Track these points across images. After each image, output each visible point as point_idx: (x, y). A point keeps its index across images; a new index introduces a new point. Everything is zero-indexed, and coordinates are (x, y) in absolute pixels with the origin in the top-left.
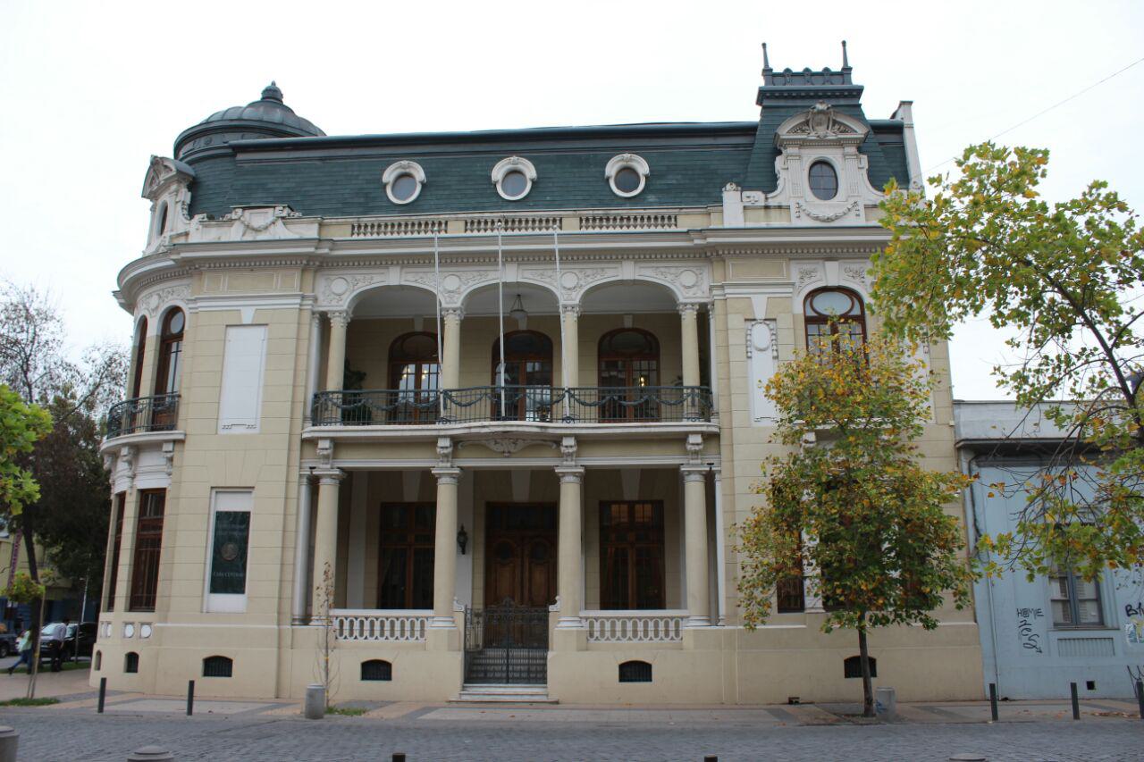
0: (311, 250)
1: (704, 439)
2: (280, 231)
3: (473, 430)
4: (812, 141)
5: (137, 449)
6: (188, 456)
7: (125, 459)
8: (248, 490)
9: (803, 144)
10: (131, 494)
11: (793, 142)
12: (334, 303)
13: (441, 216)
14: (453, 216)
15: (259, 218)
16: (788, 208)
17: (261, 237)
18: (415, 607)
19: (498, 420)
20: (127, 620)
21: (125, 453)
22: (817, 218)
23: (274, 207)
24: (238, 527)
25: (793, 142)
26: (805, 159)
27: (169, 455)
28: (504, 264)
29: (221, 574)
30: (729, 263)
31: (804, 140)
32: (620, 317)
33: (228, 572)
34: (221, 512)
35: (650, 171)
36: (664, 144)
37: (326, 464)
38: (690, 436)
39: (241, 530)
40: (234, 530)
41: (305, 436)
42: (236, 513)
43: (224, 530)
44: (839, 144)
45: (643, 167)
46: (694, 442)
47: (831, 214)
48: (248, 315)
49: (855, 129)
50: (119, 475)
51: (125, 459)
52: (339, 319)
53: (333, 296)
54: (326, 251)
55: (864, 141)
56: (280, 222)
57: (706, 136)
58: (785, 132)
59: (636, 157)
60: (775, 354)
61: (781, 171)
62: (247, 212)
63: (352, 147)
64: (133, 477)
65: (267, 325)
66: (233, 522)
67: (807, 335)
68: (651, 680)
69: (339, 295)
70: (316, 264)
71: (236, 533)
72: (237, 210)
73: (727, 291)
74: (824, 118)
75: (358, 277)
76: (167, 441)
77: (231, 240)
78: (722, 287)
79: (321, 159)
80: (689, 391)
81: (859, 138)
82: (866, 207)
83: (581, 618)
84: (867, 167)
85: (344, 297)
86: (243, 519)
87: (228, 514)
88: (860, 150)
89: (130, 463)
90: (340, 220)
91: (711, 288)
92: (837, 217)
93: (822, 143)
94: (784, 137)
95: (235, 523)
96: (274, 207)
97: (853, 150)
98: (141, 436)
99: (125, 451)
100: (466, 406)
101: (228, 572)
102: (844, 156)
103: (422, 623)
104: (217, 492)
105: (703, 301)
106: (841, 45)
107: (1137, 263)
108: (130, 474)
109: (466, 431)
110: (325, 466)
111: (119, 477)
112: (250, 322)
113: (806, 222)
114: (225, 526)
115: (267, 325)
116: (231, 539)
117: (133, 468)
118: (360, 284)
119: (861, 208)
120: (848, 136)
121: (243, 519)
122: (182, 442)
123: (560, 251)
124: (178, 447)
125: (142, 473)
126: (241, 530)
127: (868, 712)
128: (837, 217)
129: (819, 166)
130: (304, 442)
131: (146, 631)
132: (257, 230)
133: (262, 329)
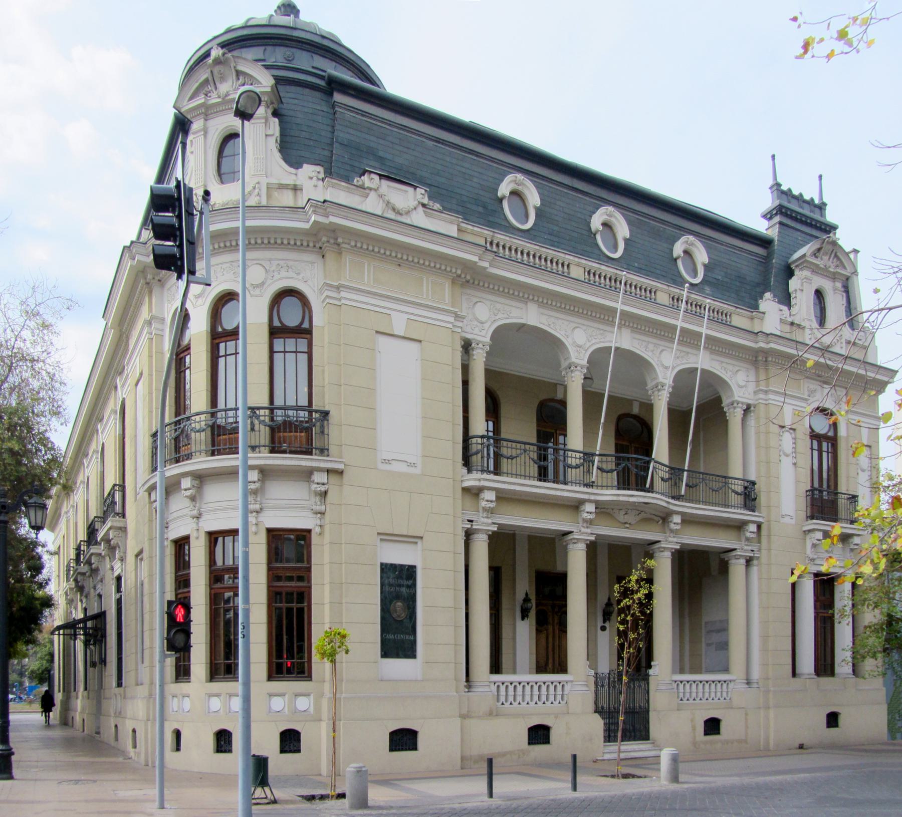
1: (497, 497)
2: (419, 218)
3: (621, 498)
5: (201, 478)
6: (342, 495)
7: (188, 493)
8: (414, 539)
10: (197, 538)
12: (476, 331)
13: (567, 257)
14: (576, 259)
15: (406, 198)
17: (399, 218)
18: (553, 672)
19: (642, 490)
21: (189, 486)
23: (415, 187)
24: (406, 583)
27: (323, 488)
28: (620, 328)
29: (391, 637)
30: (347, 258)
32: (630, 402)
33: (398, 638)
34: (386, 564)
35: (541, 204)
36: (662, 217)
37: (488, 517)
38: (315, 473)
39: (408, 587)
40: (400, 586)
41: (466, 484)
43: (390, 585)
45: (534, 198)
48: (399, 325)
50: (175, 515)
51: (188, 493)
52: (480, 351)
53: (476, 323)
54: (486, 265)
56: (420, 209)
57: (717, 230)
59: (699, 244)
60: (794, 461)
62: (385, 183)
63: (743, 240)
64: (198, 517)
66: (399, 577)
69: (484, 318)
70: (468, 279)
71: (404, 590)
72: (373, 176)
73: (771, 396)
75: (498, 306)
76: (320, 470)
77: (363, 209)
78: (766, 392)
83: (490, 682)
85: (486, 326)
86: (409, 573)
87: (393, 567)
89: (193, 499)
90: (476, 229)
91: (755, 393)
95: (402, 578)
96: (415, 187)
98: (202, 462)
99: (186, 483)
100: (608, 472)
101: (398, 638)
103: (563, 686)
104: (381, 540)
105: (750, 402)
106: (770, 159)
107: (3, 361)
108: (195, 512)
109: (615, 498)
110: (486, 520)
111: (175, 519)
114: (392, 581)
115: (420, 341)
116: (398, 597)
117: (197, 505)
118: (500, 316)
121: (409, 573)
122: (340, 473)
123: (682, 328)
124: (334, 479)
125: (210, 511)
126: (408, 587)
130: (466, 490)
132: (399, 213)
133: (414, 346)
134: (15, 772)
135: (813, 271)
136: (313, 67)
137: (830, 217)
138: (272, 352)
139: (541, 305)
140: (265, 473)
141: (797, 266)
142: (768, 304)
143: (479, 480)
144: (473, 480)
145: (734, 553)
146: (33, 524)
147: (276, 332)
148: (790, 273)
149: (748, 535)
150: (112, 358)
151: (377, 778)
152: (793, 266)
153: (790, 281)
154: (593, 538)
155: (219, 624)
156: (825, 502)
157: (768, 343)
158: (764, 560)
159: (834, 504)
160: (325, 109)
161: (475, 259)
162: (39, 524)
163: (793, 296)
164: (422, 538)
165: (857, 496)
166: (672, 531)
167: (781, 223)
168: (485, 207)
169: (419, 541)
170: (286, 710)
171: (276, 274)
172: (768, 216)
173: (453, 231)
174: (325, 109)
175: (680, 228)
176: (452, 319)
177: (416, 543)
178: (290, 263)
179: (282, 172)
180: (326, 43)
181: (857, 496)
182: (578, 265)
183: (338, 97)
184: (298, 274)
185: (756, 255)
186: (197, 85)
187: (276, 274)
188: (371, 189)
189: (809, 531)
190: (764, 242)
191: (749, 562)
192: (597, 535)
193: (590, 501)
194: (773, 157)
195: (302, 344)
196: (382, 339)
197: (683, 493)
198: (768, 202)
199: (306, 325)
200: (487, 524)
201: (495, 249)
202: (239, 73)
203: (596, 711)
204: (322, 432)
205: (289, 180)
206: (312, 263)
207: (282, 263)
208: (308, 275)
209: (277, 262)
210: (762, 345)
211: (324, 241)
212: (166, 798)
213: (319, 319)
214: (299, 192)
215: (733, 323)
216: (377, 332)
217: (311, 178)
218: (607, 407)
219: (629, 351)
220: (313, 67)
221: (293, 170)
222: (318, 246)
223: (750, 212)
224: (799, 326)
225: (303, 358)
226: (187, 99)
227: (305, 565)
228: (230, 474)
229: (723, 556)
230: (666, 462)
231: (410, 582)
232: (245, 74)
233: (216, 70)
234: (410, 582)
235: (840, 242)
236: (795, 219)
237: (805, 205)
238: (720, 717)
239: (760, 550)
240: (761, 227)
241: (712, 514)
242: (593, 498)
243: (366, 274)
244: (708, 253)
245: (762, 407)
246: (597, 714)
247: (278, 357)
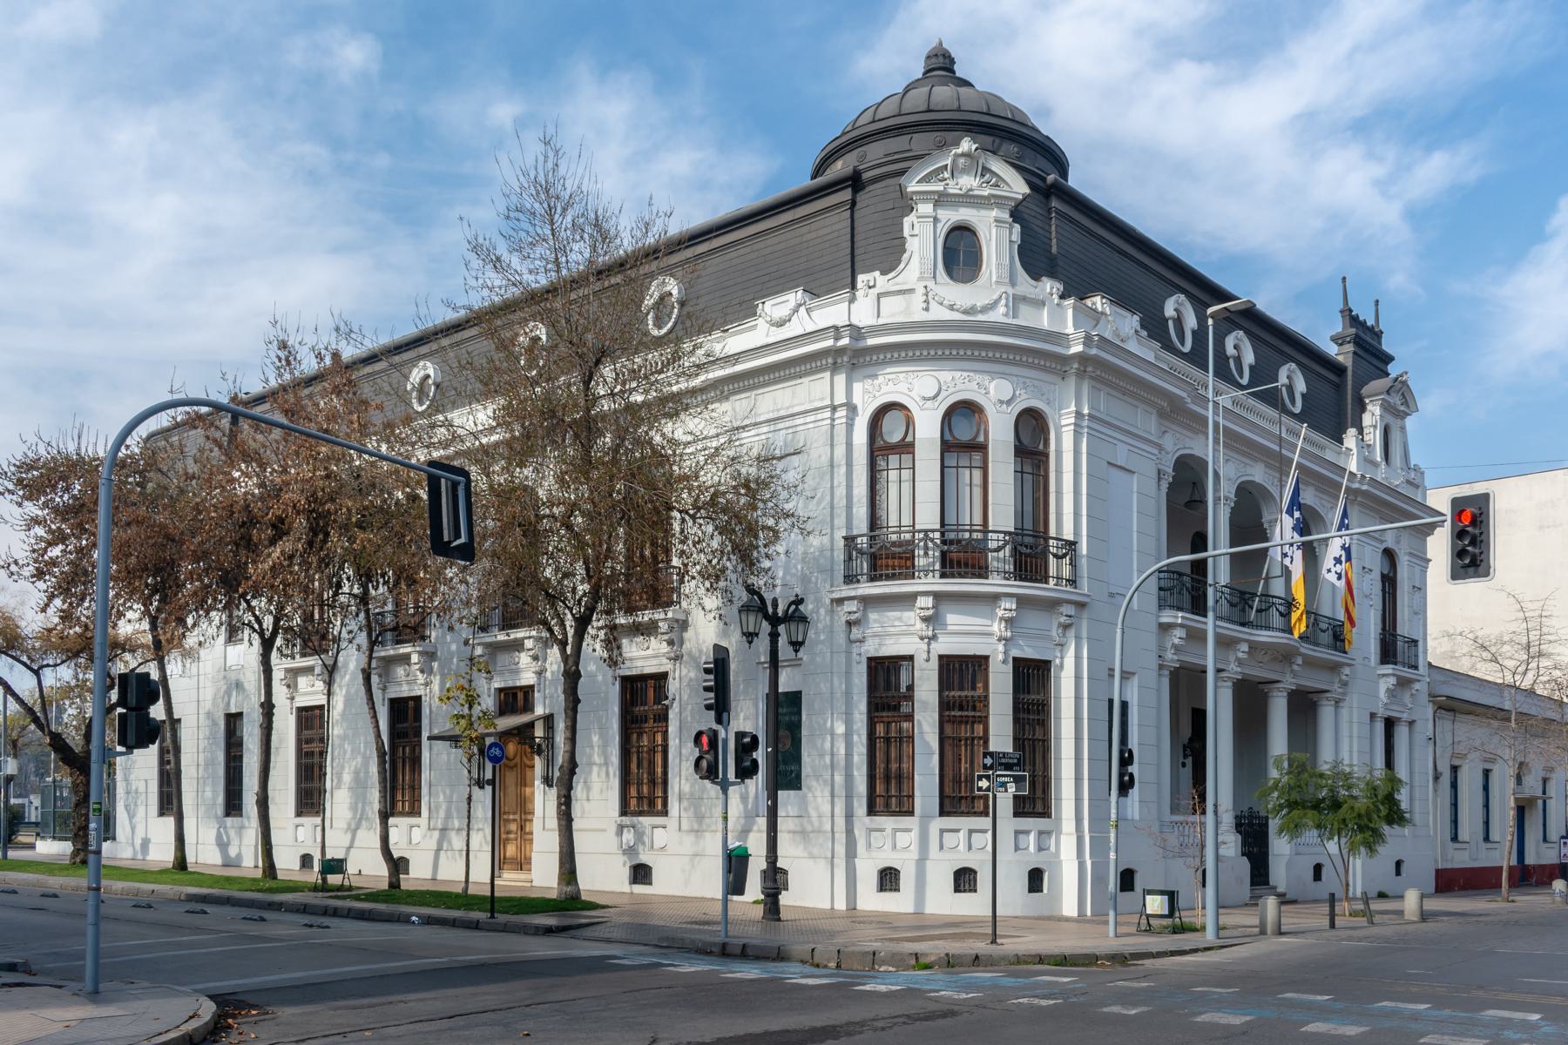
2: (1132, 346)
35: (1052, 275)
138: (943, 467)
140: (938, 597)
147: (947, 447)
150: (407, 344)
161: (1184, 395)
167: (1355, 353)
172: (1338, 340)
173: (1150, 357)
175: (1282, 352)
190: (1339, 370)
195: (977, 457)
199: (981, 439)
202: (986, 170)
218: (1088, 475)
225: (977, 474)
227: (979, 692)
228: (908, 599)
232: (994, 174)
236: (1367, 351)
247: (951, 473)
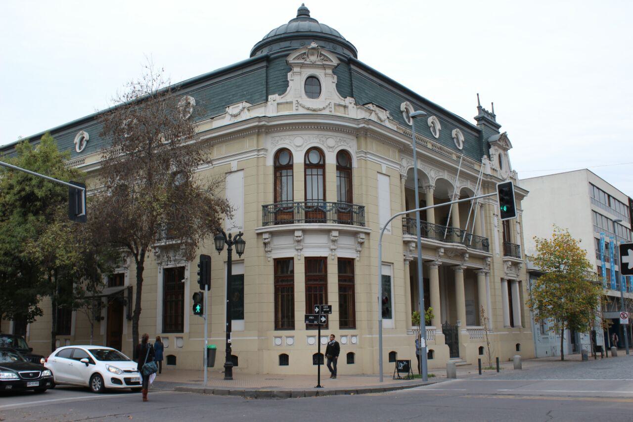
0: (256, 124)
2: (246, 115)
4: (308, 64)
9: (302, 66)
11: (297, 65)
16: (291, 103)
17: (239, 119)
20: (352, 334)
22: (308, 109)
25: (297, 65)
26: (303, 75)
30: (369, 140)
31: (303, 64)
42: (386, 276)
44: (324, 67)
46: (335, 235)
47: (315, 107)
48: (234, 165)
49: (332, 60)
55: (336, 67)
58: (292, 59)
61: (290, 81)
65: (243, 169)
67: (305, 175)
68: (288, 364)
73: (491, 201)
74: (316, 52)
79: (380, 85)
80: (296, 205)
81: (334, 66)
82: (335, 104)
84: (336, 82)
88: (334, 73)
92: (320, 110)
93: (313, 65)
94: (291, 62)
96: (386, 110)
97: (330, 71)
102: (326, 74)
105: (482, 202)
106: (476, 95)
109: (452, 247)
112: (236, 170)
113: (302, 111)
115: (243, 169)
119: (332, 106)
120: (327, 63)
123: (461, 171)
127: (563, 359)
128: (320, 110)
129: (311, 79)
130: (404, 242)
131: (354, 340)
132: (235, 116)
133: (387, 178)
134: (234, 376)
135: (498, 147)
136: (343, 53)
137: (498, 121)
139: (449, 172)
141: (492, 144)
142: (485, 159)
143: (411, 238)
144: (408, 237)
145: (433, 263)
146: (218, 248)
148: (489, 147)
149: (411, 248)
151: (542, 359)
152: (491, 144)
153: (490, 150)
154: (412, 259)
155: (279, 301)
156: (509, 248)
157: (491, 179)
158: (492, 274)
159: (350, 213)
160: (347, 70)
162: (221, 248)
163: (491, 156)
164: (393, 263)
165: (364, 207)
166: (439, 256)
168: (362, 100)
169: (392, 265)
170: (358, 343)
171: (339, 143)
172: (476, 119)
174: (347, 70)
176: (399, 167)
177: (390, 265)
178: (345, 139)
179: (337, 98)
180: (348, 44)
181: (364, 207)
182: (430, 142)
183: (352, 67)
184: (348, 144)
185: (476, 136)
186: (299, 54)
187: (339, 143)
188: (373, 110)
189: (506, 261)
191: (486, 273)
192: (414, 257)
193: (443, 247)
194: (492, 103)
196: (379, 175)
197: (470, 244)
198: (476, 113)
200: (411, 257)
201: (407, 135)
203: (446, 344)
204: (362, 215)
205: (343, 103)
206: (353, 140)
207: (341, 138)
208: (351, 146)
209: (339, 138)
210: (489, 180)
211: (362, 133)
212: (482, 367)
213: (355, 164)
214: (346, 108)
215: (475, 168)
216: (378, 172)
217: (351, 103)
219: (470, 189)
220: (343, 53)
221: (343, 98)
222: (357, 133)
223: (470, 116)
224: (496, 170)
226: (293, 58)
227: (323, 273)
229: (451, 268)
230: (459, 227)
231: (389, 284)
233: (310, 51)
234: (389, 284)
235: (508, 136)
237: (489, 116)
238: (396, 351)
239: (490, 269)
240: (474, 123)
241: (478, 253)
242: (444, 246)
243: (373, 147)
244: (464, 136)
245: (487, 206)
246: (447, 345)
